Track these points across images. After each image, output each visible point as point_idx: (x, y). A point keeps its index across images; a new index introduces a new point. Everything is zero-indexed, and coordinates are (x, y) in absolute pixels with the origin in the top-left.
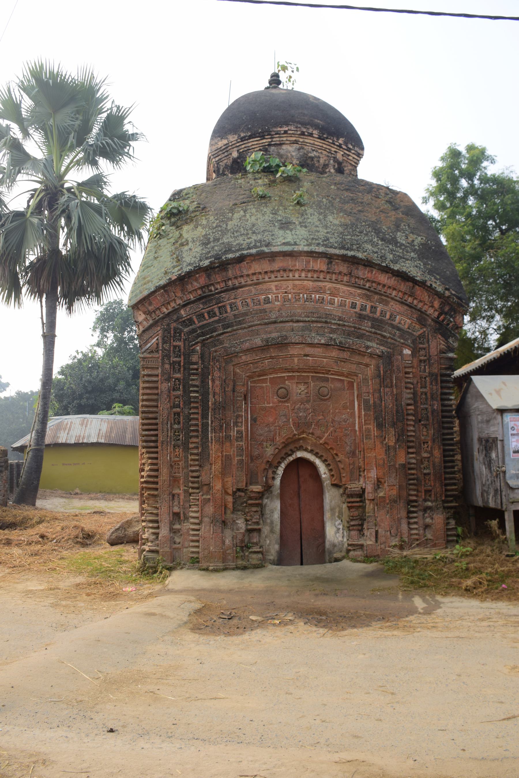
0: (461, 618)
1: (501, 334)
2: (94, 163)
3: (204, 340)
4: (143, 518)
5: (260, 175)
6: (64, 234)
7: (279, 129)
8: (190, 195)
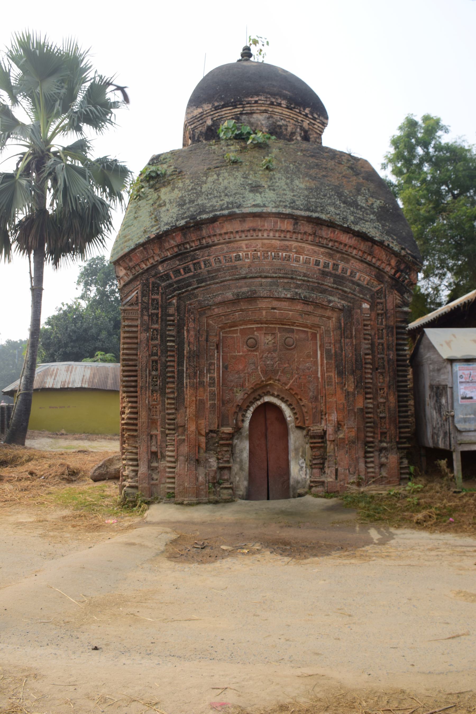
0: (412, 548)
1: (452, 290)
2: (79, 129)
3: (180, 294)
4: (124, 456)
5: (232, 142)
7: (250, 99)
8: (167, 160)
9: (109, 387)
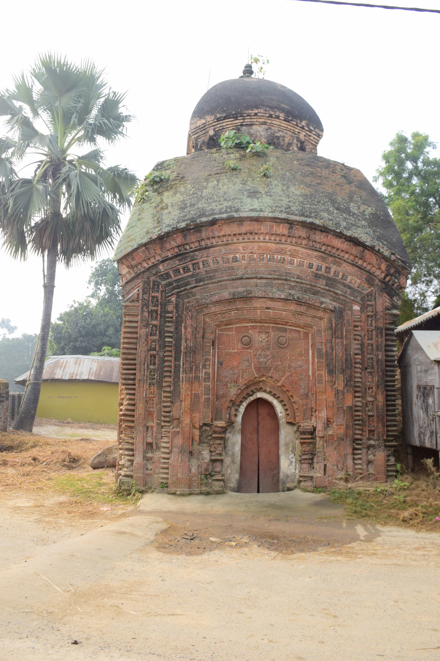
0: (398, 547)
1: (438, 296)
2: (92, 140)
3: (179, 292)
4: (121, 446)
5: (232, 151)
6: (65, 199)
7: (250, 112)
8: (171, 166)
9: (114, 381)
